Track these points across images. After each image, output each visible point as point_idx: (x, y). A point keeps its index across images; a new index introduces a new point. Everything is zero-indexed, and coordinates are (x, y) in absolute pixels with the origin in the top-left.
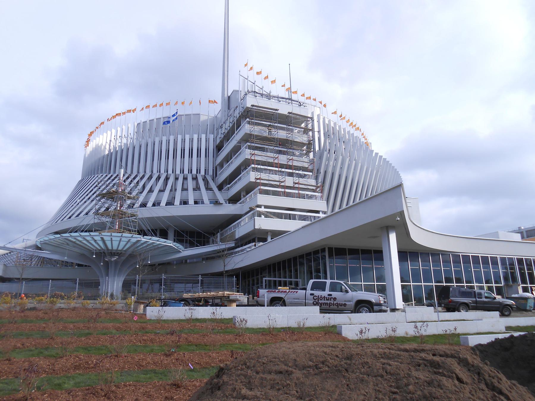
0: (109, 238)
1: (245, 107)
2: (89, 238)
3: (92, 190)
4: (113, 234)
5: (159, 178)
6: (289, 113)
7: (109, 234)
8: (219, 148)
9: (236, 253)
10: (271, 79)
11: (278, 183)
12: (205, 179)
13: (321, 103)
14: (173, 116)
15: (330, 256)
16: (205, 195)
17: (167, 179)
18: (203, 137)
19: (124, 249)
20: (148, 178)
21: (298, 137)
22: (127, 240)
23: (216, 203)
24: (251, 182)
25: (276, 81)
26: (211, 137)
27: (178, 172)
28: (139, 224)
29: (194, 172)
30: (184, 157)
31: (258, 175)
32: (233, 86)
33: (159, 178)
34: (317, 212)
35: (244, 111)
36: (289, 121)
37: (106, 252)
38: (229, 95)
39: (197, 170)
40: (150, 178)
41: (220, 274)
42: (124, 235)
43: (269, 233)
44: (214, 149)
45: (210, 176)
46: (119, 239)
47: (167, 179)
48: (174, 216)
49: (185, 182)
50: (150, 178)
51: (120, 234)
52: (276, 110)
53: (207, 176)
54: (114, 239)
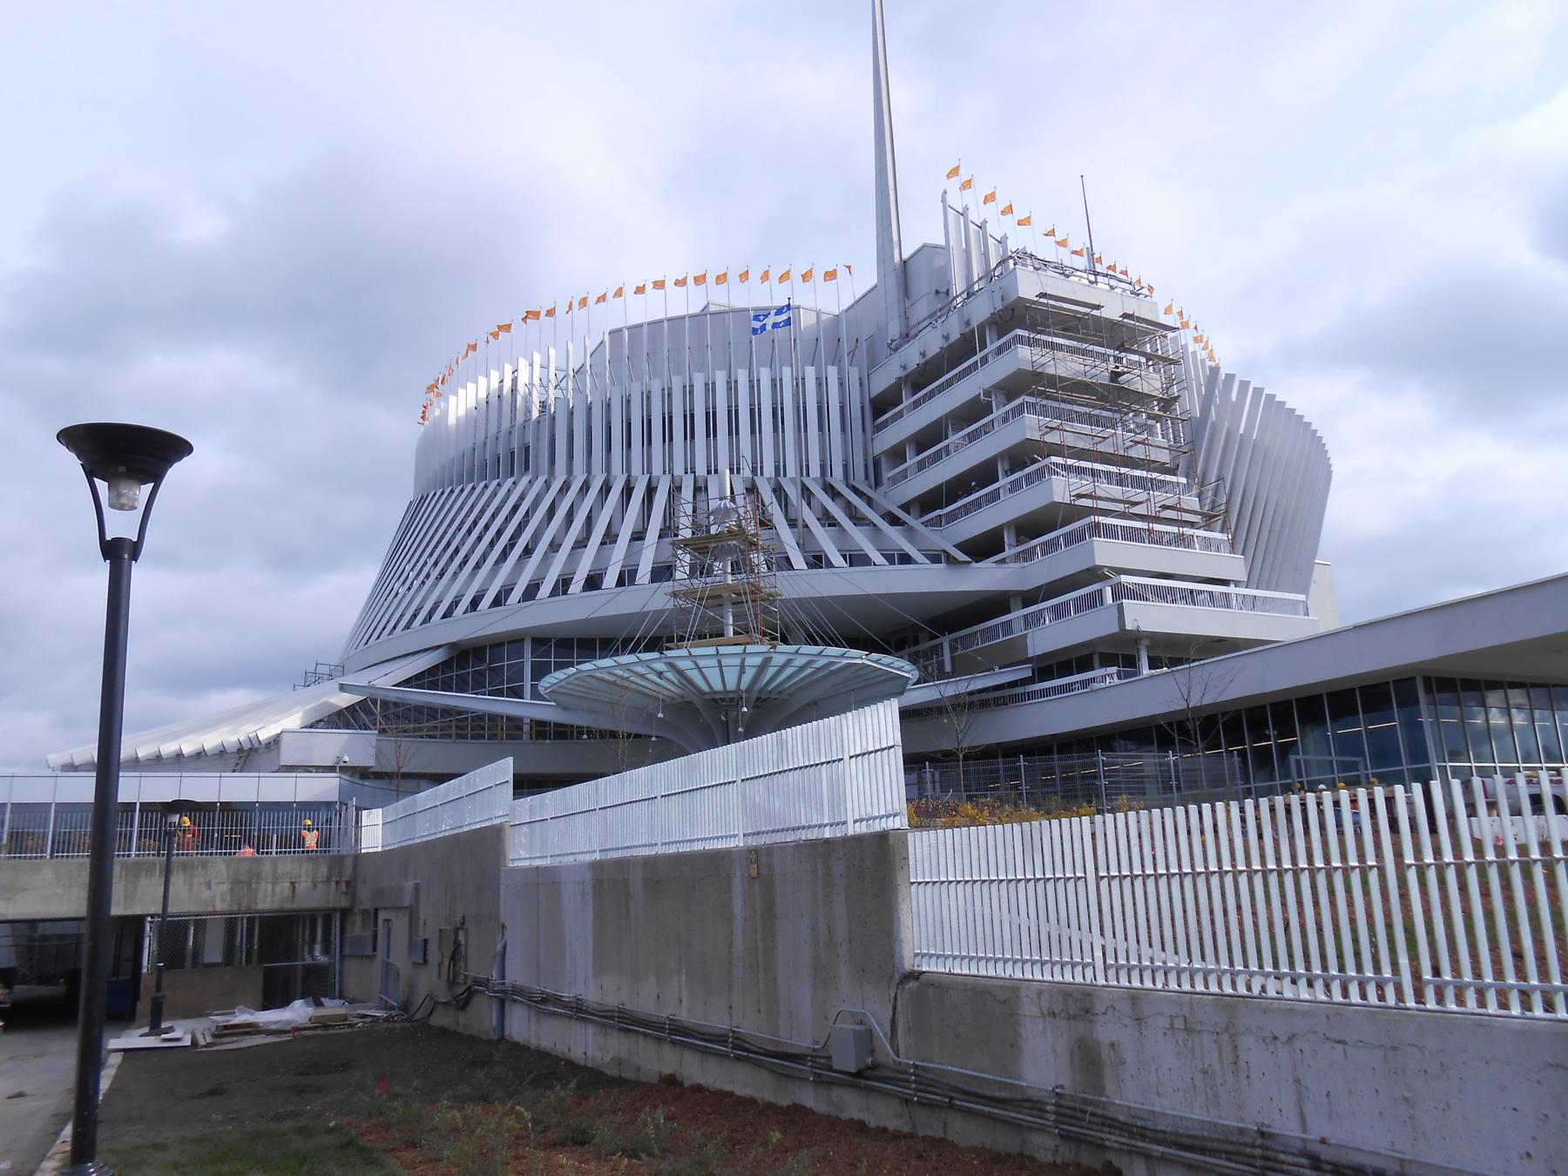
0: (714, 662)
1: (1013, 298)
2: (660, 666)
3: (462, 523)
4: (723, 650)
5: (606, 489)
6: (1125, 316)
7: (712, 650)
8: (882, 406)
9: (1031, 695)
10: (1019, 214)
11: (1120, 507)
12: (778, 491)
13: (659, 285)
14: (779, 311)
15: (1428, 690)
16: (860, 539)
17: (651, 490)
18: (832, 372)
19: (744, 686)
20: (561, 490)
21: (1150, 382)
22: (758, 660)
23: (856, 559)
24: (1055, 505)
25: (1033, 220)
26: (854, 375)
27: (679, 470)
28: (782, 618)
29: (701, 470)
30: (671, 439)
31: (1084, 484)
32: (920, 229)
33: (606, 489)
34: (1225, 582)
35: (1005, 309)
36: (1122, 335)
37: (696, 700)
38: (905, 256)
39: (777, 468)
40: (585, 488)
41: (1012, 750)
42: (750, 649)
43: (1146, 642)
44: (862, 408)
45: (769, 480)
46: (737, 661)
47: (651, 490)
48: (868, 596)
49: (701, 496)
50: (585, 488)
51: (739, 649)
52: (1098, 307)
53: (782, 479)
54: (724, 662)
